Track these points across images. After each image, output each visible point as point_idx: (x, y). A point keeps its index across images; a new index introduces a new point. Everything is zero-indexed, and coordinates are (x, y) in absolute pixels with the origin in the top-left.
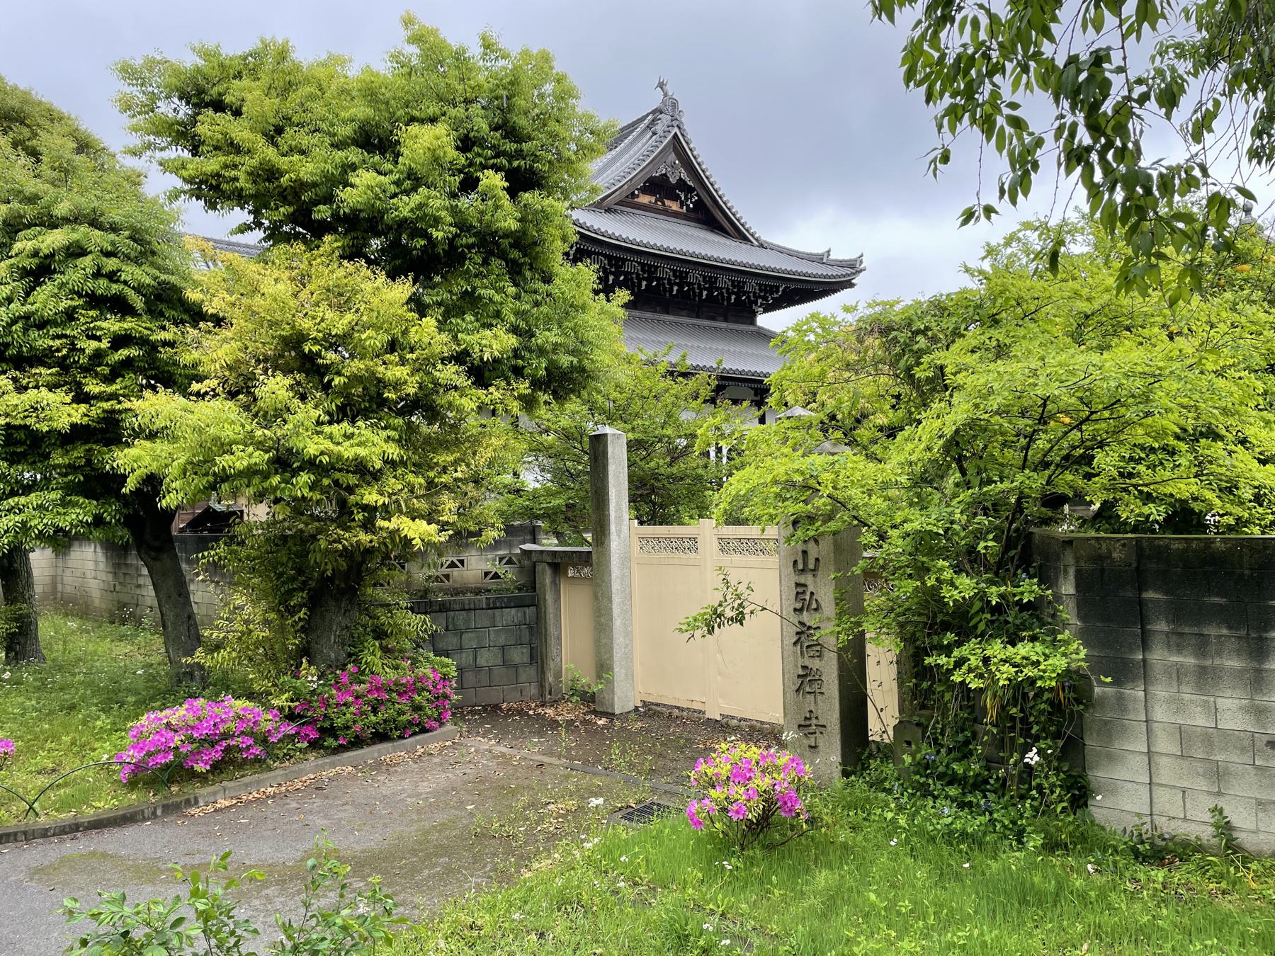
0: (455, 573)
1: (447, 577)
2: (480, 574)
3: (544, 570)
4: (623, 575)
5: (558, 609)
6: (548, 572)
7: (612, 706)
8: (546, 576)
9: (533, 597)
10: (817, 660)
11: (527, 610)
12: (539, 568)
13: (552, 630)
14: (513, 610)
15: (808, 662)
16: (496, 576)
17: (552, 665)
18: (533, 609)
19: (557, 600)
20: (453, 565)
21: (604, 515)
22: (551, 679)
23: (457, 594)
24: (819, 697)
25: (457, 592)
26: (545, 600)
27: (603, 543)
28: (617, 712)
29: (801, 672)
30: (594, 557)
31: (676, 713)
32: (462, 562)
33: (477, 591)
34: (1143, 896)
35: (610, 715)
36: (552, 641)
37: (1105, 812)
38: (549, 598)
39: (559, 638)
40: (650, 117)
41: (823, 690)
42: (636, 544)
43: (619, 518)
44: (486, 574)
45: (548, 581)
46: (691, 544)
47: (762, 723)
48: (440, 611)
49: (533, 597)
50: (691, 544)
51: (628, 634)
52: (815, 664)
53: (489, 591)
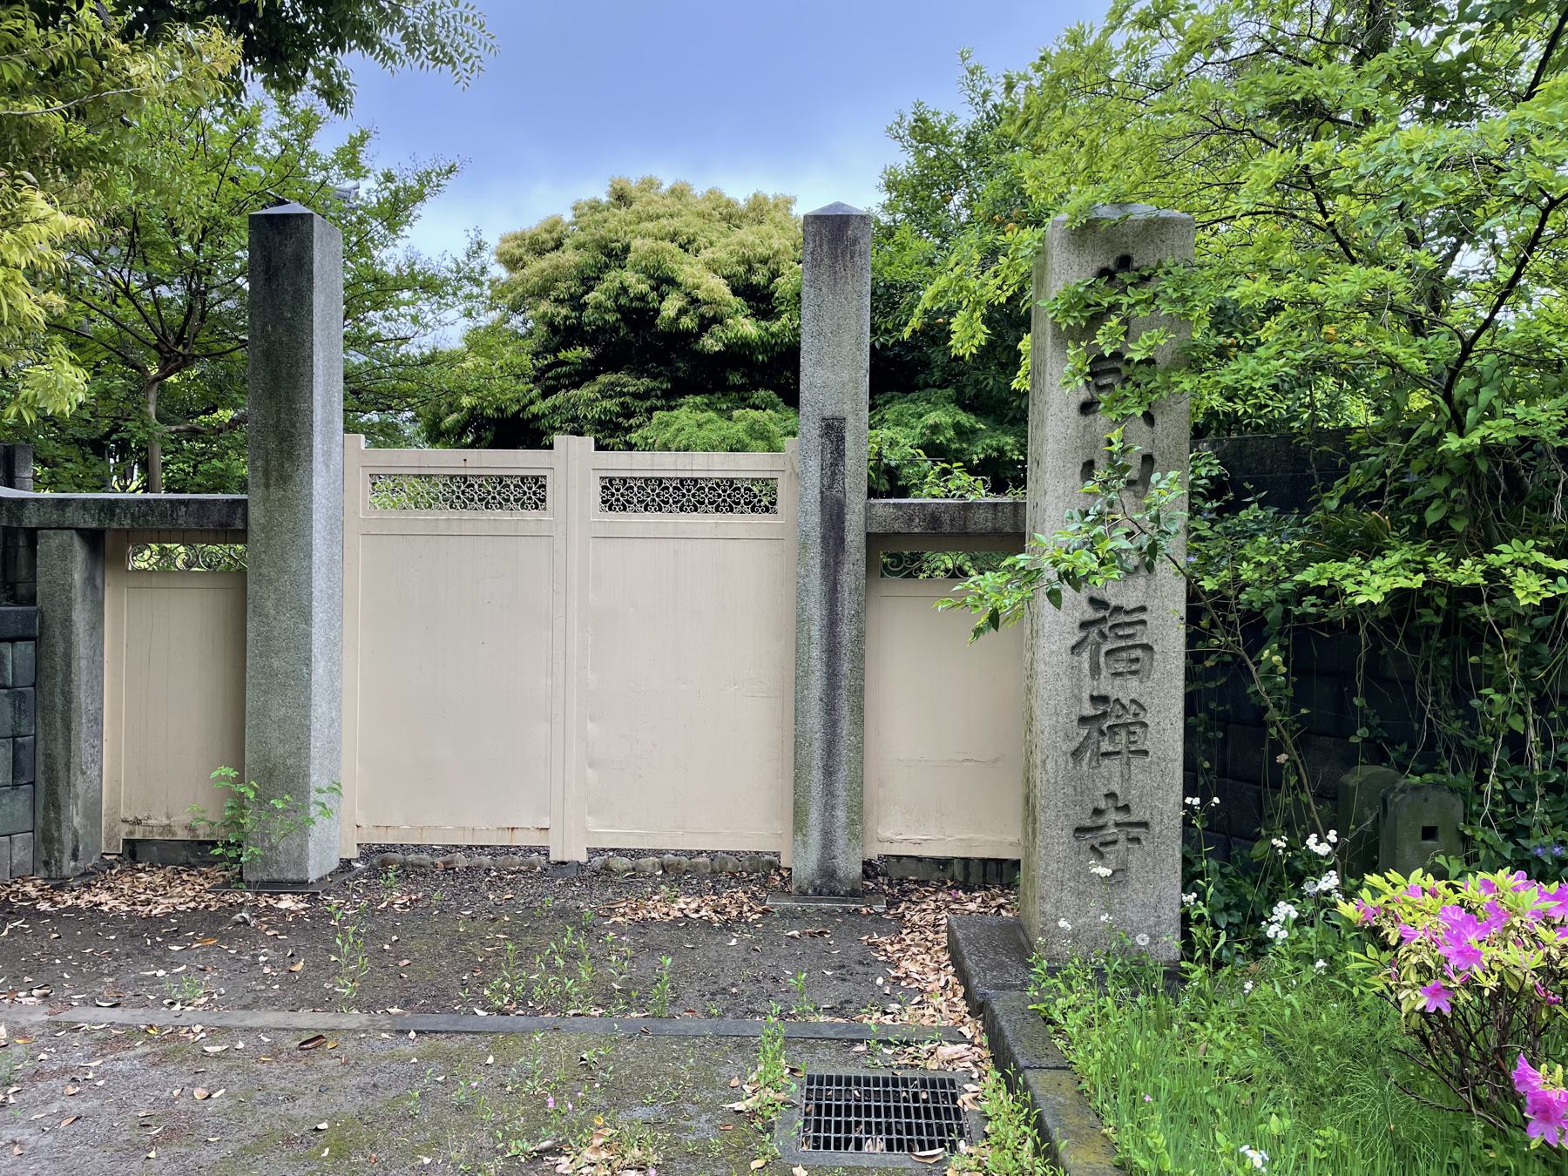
3: (65, 553)
4: (331, 560)
6: (79, 552)
7: (300, 863)
9: (30, 618)
10: (1133, 682)
13: (82, 697)
15: (1106, 686)
17: (80, 785)
18: (25, 648)
19: (97, 625)
21: (293, 411)
22: (77, 821)
24: (1136, 761)
26: (67, 623)
27: (284, 479)
28: (313, 876)
29: (1088, 710)
30: (255, 513)
31: (461, 861)
34: (201, 1026)
35: (297, 886)
36: (82, 727)
39: (97, 721)
41: (1147, 745)
42: (362, 483)
43: (328, 422)
45: (78, 577)
46: (533, 492)
47: (691, 854)
49: (30, 618)
50: (533, 492)
51: (335, 695)
52: (1126, 690)
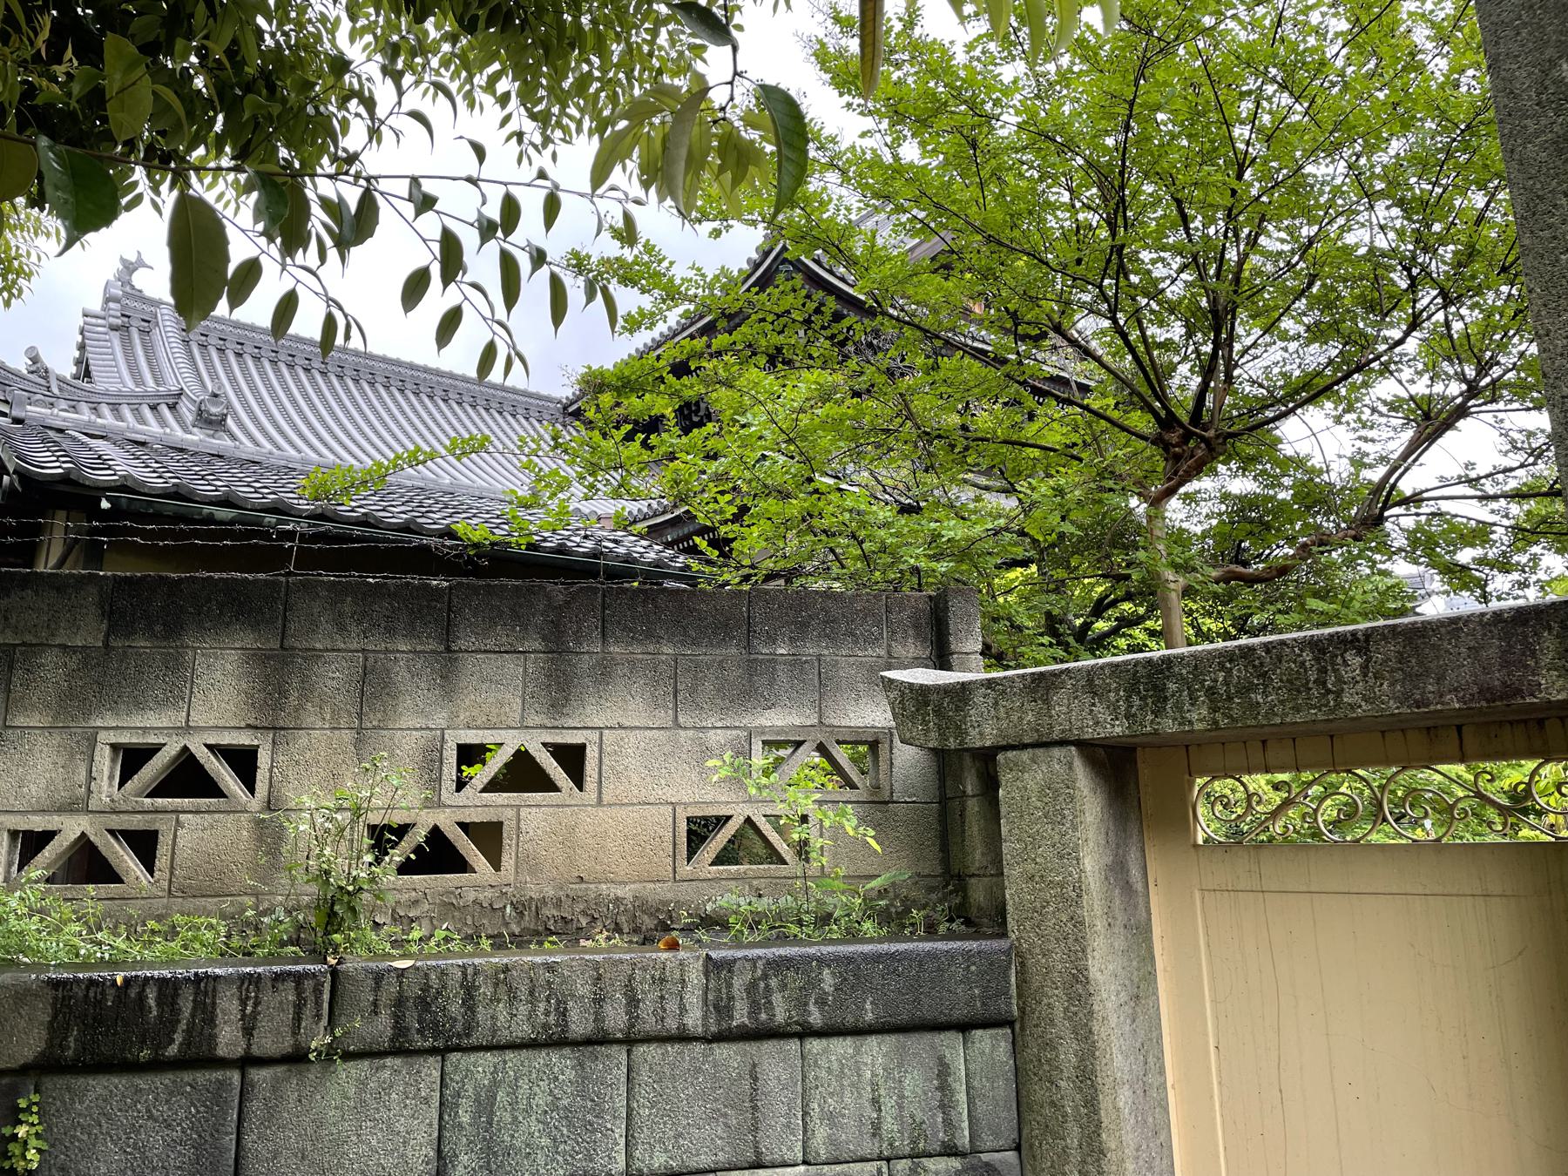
0: (529, 816)
1: (488, 836)
2: (664, 828)
5: (1141, 991)
8: (1059, 826)
9: (995, 969)
11: (951, 1046)
12: (1023, 782)
14: (875, 1051)
16: (747, 845)
18: (991, 1045)
20: (522, 775)
23: (540, 934)
25: (542, 924)
26: (1078, 983)
32: (572, 758)
33: (655, 926)
37: (428, 648)
38: (1104, 967)
40: (1139, 887)
44: (699, 831)
48: (399, 1048)
53: (714, 922)
